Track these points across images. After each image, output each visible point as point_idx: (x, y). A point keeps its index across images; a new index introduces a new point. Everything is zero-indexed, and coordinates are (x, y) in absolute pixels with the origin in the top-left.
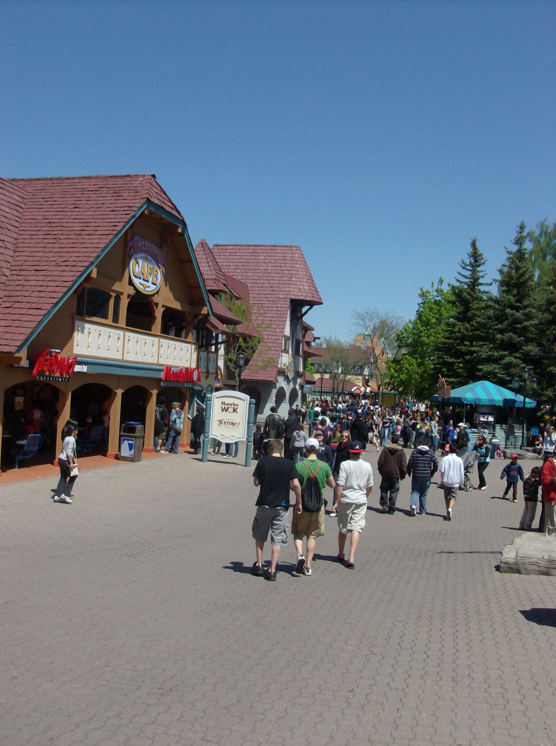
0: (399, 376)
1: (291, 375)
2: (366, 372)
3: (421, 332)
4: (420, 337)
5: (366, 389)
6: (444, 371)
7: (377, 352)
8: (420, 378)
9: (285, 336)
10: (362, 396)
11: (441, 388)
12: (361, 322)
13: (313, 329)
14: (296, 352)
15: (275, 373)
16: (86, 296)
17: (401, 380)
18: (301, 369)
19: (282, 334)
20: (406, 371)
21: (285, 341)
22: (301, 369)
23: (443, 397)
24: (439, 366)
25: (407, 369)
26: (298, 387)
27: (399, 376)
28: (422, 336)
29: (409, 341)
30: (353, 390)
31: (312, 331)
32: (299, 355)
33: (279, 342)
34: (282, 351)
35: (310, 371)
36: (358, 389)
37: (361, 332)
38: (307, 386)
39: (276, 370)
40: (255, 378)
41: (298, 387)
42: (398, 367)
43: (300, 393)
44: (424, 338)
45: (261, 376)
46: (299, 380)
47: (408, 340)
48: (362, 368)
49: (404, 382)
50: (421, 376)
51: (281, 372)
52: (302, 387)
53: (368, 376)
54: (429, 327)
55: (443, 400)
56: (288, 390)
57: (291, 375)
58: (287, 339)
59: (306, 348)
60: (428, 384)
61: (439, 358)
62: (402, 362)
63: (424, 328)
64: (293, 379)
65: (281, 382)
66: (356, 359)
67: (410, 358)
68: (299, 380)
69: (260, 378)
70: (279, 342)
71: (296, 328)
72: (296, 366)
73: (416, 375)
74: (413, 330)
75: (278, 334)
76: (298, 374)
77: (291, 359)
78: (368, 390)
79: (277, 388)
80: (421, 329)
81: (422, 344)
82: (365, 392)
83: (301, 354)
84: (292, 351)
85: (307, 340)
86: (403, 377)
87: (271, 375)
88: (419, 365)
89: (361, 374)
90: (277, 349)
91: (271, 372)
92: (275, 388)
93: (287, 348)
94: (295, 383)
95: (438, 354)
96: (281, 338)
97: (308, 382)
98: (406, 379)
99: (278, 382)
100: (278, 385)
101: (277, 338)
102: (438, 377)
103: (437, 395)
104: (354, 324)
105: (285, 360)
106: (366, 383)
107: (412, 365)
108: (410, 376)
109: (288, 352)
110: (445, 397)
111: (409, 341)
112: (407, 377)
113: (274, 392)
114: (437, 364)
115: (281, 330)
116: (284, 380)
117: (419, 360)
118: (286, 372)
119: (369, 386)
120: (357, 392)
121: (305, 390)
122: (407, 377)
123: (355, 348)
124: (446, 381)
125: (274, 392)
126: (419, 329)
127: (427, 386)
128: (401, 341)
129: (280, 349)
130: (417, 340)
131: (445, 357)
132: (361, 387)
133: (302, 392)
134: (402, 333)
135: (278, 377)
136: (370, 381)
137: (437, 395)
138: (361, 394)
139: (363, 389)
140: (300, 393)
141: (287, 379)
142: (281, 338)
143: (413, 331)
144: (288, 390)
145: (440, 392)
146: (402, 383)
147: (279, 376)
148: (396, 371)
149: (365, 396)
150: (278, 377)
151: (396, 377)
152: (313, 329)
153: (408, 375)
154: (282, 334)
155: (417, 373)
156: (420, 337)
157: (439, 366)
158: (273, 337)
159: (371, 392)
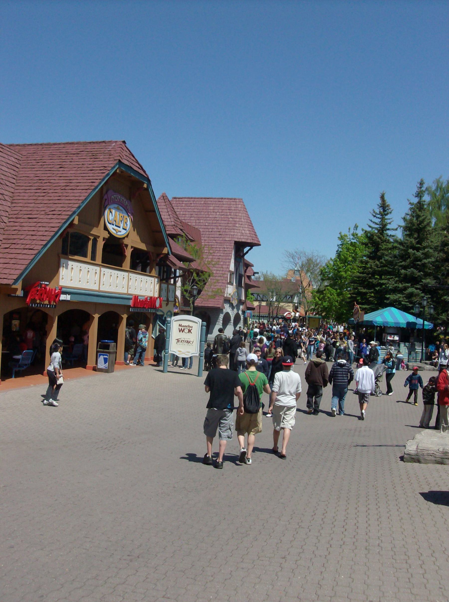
0: (322, 303)
1: (235, 303)
2: (296, 300)
3: (340, 268)
4: (339, 272)
5: (295, 314)
6: (358, 300)
7: (305, 284)
8: (339, 305)
9: (230, 271)
10: (293, 319)
11: (356, 313)
12: (292, 260)
13: (253, 266)
14: (239, 284)
15: (222, 301)
17: (324, 306)
18: (243, 298)
19: (228, 270)
20: (328, 299)
21: (230, 275)
22: (243, 298)
23: (358, 320)
24: (354, 295)
25: (329, 298)
26: (240, 312)
27: (322, 303)
28: (341, 271)
29: (330, 276)
30: (285, 315)
31: (252, 267)
32: (241, 286)
33: (226, 276)
34: (228, 284)
35: (250, 299)
36: (289, 314)
37: (291, 268)
38: (248, 311)
39: (223, 298)
40: (206, 305)
41: (240, 312)
42: (322, 296)
43: (242, 317)
44: (343, 273)
45: (211, 304)
46: (241, 307)
47: (329, 274)
48: (292, 297)
49: (326, 308)
50: (340, 304)
51: (227, 301)
52: (244, 312)
53: (298, 303)
54: (346, 264)
55: (358, 323)
56: (232, 315)
57: (235, 303)
58: (232, 273)
59: (247, 281)
60: (346, 310)
61: (354, 289)
62: (324, 292)
63: (342, 265)
64: (236, 305)
65: (227, 309)
66: (287, 290)
67: (331, 289)
68: (241, 307)
69: (210, 305)
70: (226, 276)
71: (239, 265)
72: (239, 295)
73: (336, 303)
74: (333, 266)
75: (224, 269)
76: (241, 302)
77: (235, 290)
78: (297, 314)
79: (224, 314)
80: (340, 265)
81: (341, 277)
82: (295, 316)
83: (243, 285)
84: (236, 283)
85: (248, 275)
86: (325, 304)
87: (219, 303)
88: (338, 295)
89: (292, 302)
90: (224, 281)
91: (219, 300)
92: (222, 313)
93: (232, 281)
94: (238, 309)
95: (354, 286)
96: (227, 273)
97: (249, 309)
98: (328, 306)
99: (224, 308)
100: (225, 311)
101: (223, 272)
102: (354, 305)
103: (353, 319)
104: (286, 261)
105: (231, 290)
106: (296, 309)
107: (332, 294)
108: (331, 303)
109: (232, 284)
110: (360, 321)
111: (330, 276)
112: (328, 304)
113: (221, 316)
114: (353, 294)
115: (227, 266)
116: (230, 306)
117: (338, 291)
118: (231, 300)
119: (298, 312)
120: (288, 316)
121: (246, 314)
122: (328, 304)
123: (286, 281)
124: (360, 307)
125: (221, 316)
126: (338, 265)
127: (345, 311)
128: (324, 275)
129: (226, 282)
130: (337, 274)
131: (359, 288)
132: (291, 313)
133: (244, 317)
134: (325, 269)
135: (225, 305)
136: (299, 307)
137: (353, 319)
138: (292, 318)
139: (293, 314)
140: (242, 317)
141: (232, 306)
142: (227, 273)
143: (334, 267)
144: (232, 315)
145: (356, 316)
146: (324, 309)
147: (225, 303)
148: (320, 300)
149: (295, 320)
150: (225, 305)
151: (320, 305)
152: (253, 266)
153: (329, 303)
154: (228, 270)
155: (337, 301)
156: (339, 272)
157: (354, 295)
158: (221, 272)
159: (300, 316)
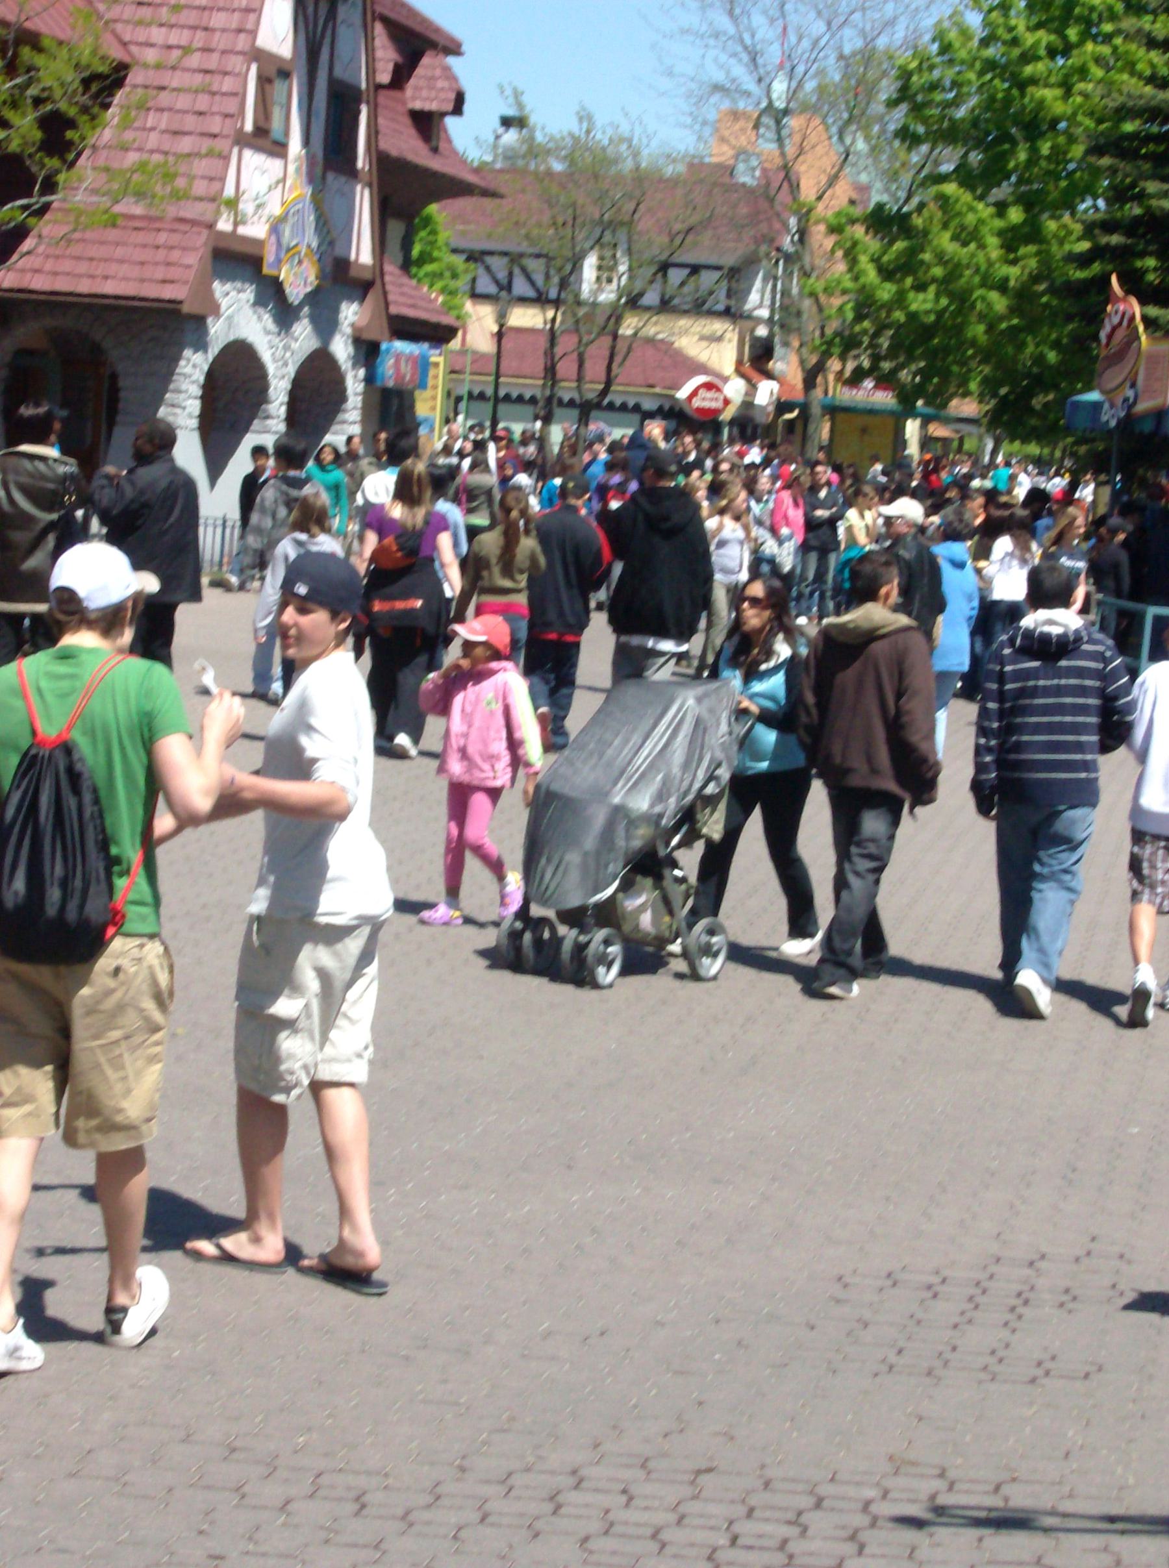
0: (900, 300)
1: (299, 280)
2: (758, 300)
3: (1028, 57)
4: (1022, 85)
5: (753, 387)
6: (1144, 272)
7: (808, 191)
8: (1012, 311)
9: (259, 55)
10: (732, 423)
11: (1119, 356)
12: (723, 22)
13: (453, 49)
14: (333, 155)
15: (194, 259)
16: (1063, 682)
17: (913, 316)
18: (363, 252)
19: (242, 42)
20: (938, 271)
21: (264, 81)
22: (363, 252)
23: (1130, 405)
24: (1115, 239)
25: (940, 258)
26: (341, 349)
27: (900, 300)
28: (1033, 81)
29: (961, 113)
30: (682, 394)
31: (451, 60)
32: (351, 172)
33: (228, 84)
34: (243, 141)
35: (447, 281)
36: (709, 386)
37: (719, 77)
38: (400, 346)
39: (201, 239)
40: (84, 287)
41: (341, 349)
42: (900, 245)
43: (354, 384)
44: (1049, 94)
45: (119, 279)
46: (350, 313)
47: (955, 103)
48: (737, 276)
49: (928, 332)
50: (1022, 297)
51: (238, 260)
52: (368, 351)
53: (770, 321)
54: (1072, 33)
55: (1128, 422)
56: (281, 356)
57: (299, 280)
58: (273, 73)
59: (405, 144)
60: (1056, 345)
61: (1119, 195)
62: (918, 221)
63: (1044, 37)
64: (312, 298)
65: (237, 315)
66: (701, 236)
67: (967, 197)
68: (350, 313)
69: (109, 288)
70: (228, 84)
71: (332, 14)
72: (331, 229)
73: (994, 296)
74: (985, 42)
75: (220, 41)
76: (340, 280)
77: (298, 189)
78: (766, 393)
79: (214, 350)
80: (1029, 39)
81: (1036, 126)
82: (748, 405)
83: (360, 164)
84: (306, 142)
85: (418, 105)
86: (923, 303)
87: (173, 273)
88: (1012, 240)
89: (729, 314)
90: (215, 125)
91: (175, 255)
92: (201, 345)
93: (276, 124)
94: (326, 326)
95: (1113, 171)
96: (235, 63)
97: (407, 328)
98: (940, 314)
99: (216, 310)
100: (219, 333)
101: (213, 62)
102: (1106, 296)
103: (1094, 396)
104: (685, 31)
105: (265, 191)
106: (759, 358)
107: (977, 240)
108: (962, 300)
109: (278, 149)
110: (1141, 407)
111: (961, 113)
112: (944, 302)
113: (193, 368)
114: (1108, 226)
115: (235, 20)
116: (259, 302)
117: (1015, 215)
118: (269, 257)
119: (769, 376)
120: (705, 401)
121: (387, 370)
122: (944, 302)
123: (708, 180)
124: (1146, 319)
125: (193, 368)
126: (1015, 42)
127: (1052, 356)
128: (917, 109)
129: (228, 127)
130: (1008, 101)
131: (1152, 187)
132: (726, 380)
133: (369, 380)
134: (926, 64)
135: (216, 285)
136: (779, 350)
137: (1094, 396)
138: (727, 415)
139: (735, 389)
140: (354, 384)
141: (271, 294)
142: (235, 63)
143: (990, 52)
144: (281, 356)
145: (1114, 377)
146: (916, 338)
147: (225, 277)
148: (887, 273)
149: (747, 427)
150: (218, 287)
151: (889, 307)
152: (453, 49)
153: (951, 295)
154: (242, 42)
155: (1002, 286)
156: (1022, 85)
157: (1115, 239)
158: (195, 60)
159: (782, 407)
